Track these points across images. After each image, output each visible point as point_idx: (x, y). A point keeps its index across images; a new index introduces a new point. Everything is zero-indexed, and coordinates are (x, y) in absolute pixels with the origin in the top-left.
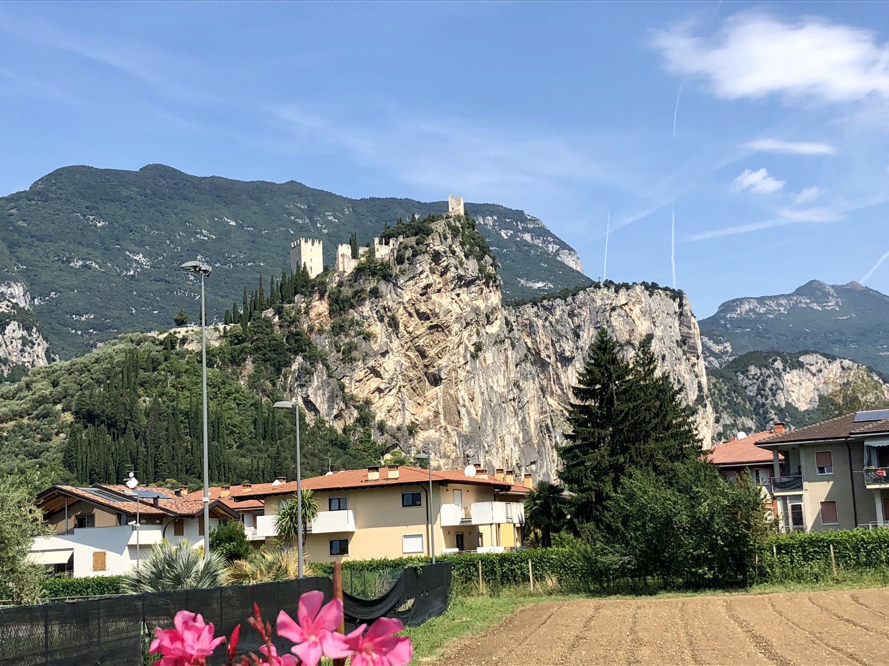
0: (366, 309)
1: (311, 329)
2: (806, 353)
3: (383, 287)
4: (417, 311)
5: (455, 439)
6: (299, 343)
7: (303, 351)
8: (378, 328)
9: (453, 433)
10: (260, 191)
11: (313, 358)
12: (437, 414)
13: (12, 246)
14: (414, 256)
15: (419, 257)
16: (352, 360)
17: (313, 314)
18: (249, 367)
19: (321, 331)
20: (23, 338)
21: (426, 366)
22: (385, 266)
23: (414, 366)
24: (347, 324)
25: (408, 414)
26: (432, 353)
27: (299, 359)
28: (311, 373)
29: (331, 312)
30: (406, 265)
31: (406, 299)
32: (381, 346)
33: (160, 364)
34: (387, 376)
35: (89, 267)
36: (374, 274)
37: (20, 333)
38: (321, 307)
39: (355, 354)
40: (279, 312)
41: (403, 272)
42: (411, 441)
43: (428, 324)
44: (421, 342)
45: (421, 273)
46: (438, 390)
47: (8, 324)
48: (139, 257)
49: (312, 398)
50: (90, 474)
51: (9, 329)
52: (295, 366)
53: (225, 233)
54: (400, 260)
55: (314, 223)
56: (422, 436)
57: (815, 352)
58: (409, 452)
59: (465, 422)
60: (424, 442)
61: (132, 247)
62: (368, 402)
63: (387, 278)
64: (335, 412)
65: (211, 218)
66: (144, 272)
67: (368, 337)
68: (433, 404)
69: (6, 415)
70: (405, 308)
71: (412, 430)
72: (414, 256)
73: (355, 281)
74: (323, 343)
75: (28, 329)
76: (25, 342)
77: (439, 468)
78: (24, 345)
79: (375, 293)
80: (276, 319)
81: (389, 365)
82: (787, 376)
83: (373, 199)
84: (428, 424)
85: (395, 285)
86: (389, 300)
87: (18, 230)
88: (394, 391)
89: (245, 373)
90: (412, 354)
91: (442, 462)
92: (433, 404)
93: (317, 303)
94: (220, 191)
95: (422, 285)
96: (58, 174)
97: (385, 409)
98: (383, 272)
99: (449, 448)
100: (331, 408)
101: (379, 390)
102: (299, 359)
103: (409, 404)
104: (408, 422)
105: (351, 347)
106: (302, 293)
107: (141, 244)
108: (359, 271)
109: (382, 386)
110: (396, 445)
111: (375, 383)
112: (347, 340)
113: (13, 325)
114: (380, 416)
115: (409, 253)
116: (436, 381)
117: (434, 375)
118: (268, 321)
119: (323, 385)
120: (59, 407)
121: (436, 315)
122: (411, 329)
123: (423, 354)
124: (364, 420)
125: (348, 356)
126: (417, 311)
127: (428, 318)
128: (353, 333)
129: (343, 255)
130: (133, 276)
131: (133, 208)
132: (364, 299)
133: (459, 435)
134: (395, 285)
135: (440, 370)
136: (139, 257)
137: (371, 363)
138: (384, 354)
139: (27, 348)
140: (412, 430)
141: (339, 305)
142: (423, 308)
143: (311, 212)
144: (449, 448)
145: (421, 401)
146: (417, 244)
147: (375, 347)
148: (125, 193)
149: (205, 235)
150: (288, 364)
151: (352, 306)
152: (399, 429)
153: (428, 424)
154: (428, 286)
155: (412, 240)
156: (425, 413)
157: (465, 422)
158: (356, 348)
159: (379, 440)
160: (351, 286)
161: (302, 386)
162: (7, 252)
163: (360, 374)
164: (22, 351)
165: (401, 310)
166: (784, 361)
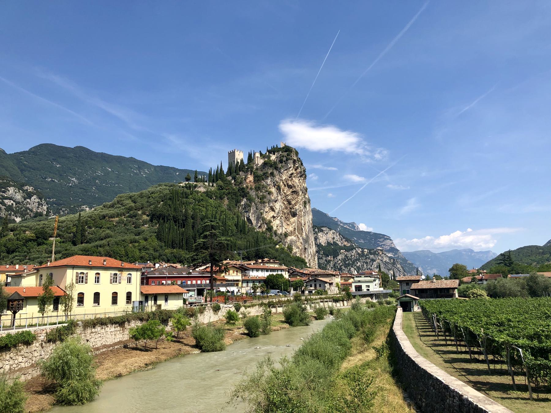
0: (269, 181)
1: (247, 187)
2: (323, 227)
3: (275, 172)
4: (287, 184)
5: (301, 241)
6: (244, 193)
7: (246, 196)
8: (273, 190)
9: (301, 238)
10: (120, 160)
11: (250, 200)
12: (295, 229)
13: (22, 171)
14: (287, 160)
15: (289, 161)
16: (264, 203)
17: (248, 181)
18: (226, 202)
19: (251, 189)
20: (38, 202)
21: (291, 208)
22: (275, 163)
23: (286, 208)
24: (261, 187)
25: (284, 228)
26: (293, 202)
27: (245, 200)
28: (250, 206)
29: (255, 181)
30: (284, 164)
31: (284, 178)
32: (275, 198)
33: (189, 195)
34: (277, 211)
35: (54, 181)
36: (271, 166)
37: (37, 200)
38: (251, 178)
39: (265, 200)
40: (234, 178)
41: (283, 167)
42: (286, 240)
43: (291, 190)
44: (289, 198)
45: (290, 168)
46: (295, 219)
47: (32, 196)
48: (74, 179)
49: (251, 218)
50: (172, 244)
51: (33, 198)
52: (243, 203)
53: (107, 173)
54: (281, 161)
55: (140, 172)
56: (289, 238)
57: (326, 227)
58: (285, 245)
59: (304, 234)
60: (290, 241)
61: (71, 175)
62: (270, 222)
63: (276, 168)
64: (259, 225)
65: (102, 167)
66: (75, 185)
67: (270, 193)
68: (294, 225)
69: (114, 214)
70: (283, 182)
71: (286, 235)
72: (287, 160)
73: (264, 168)
74: (253, 193)
75: (40, 199)
76: (39, 204)
77: (296, 253)
78: (39, 205)
79: (272, 174)
80: (233, 181)
81: (278, 206)
82: (319, 234)
83: (161, 166)
84: (292, 233)
85: (279, 172)
86: (277, 178)
87: (24, 165)
88: (279, 218)
89: (225, 203)
90: (286, 203)
91: (297, 250)
92: (294, 225)
93: (249, 176)
94: (105, 158)
95: (290, 173)
96: (41, 146)
97: (276, 225)
98: (274, 166)
99: (299, 244)
100: (257, 223)
101: (274, 217)
102: (245, 200)
103: (284, 224)
104: (284, 232)
105: (264, 197)
106: (243, 171)
107: (75, 174)
108: (265, 164)
109: (275, 215)
110: (280, 242)
111: (272, 214)
112: (261, 194)
113: (35, 197)
114: (275, 228)
115: (284, 159)
116: (294, 215)
117: (294, 212)
118: (230, 182)
119: (255, 212)
120: (140, 212)
121: (295, 187)
122: (285, 192)
123: (290, 203)
124: (270, 229)
125: (263, 201)
126: (287, 184)
127: (291, 188)
128: (264, 191)
129: (257, 157)
130: (71, 186)
131: (71, 161)
132: (268, 177)
133: (303, 239)
134: (279, 172)
135: (296, 210)
136: (74, 179)
137: (271, 205)
138: (276, 201)
139: (40, 207)
140: (286, 235)
141: (257, 179)
142: (290, 183)
143: (139, 168)
144: (299, 244)
145: (289, 223)
146: (288, 155)
147: (273, 198)
148: (68, 155)
149: (99, 173)
150: (240, 202)
151: (263, 179)
152: (281, 234)
153: (292, 233)
154: (292, 174)
155: (285, 154)
156: (290, 229)
157: (304, 234)
158: (265, 198)
159: (275, 239)
160: (262, 170)
161: (246, 212)
162: (20, 172)
163: (267, 209)
164: (38, 207)
165: (281, 183)
166: (318, 229)
